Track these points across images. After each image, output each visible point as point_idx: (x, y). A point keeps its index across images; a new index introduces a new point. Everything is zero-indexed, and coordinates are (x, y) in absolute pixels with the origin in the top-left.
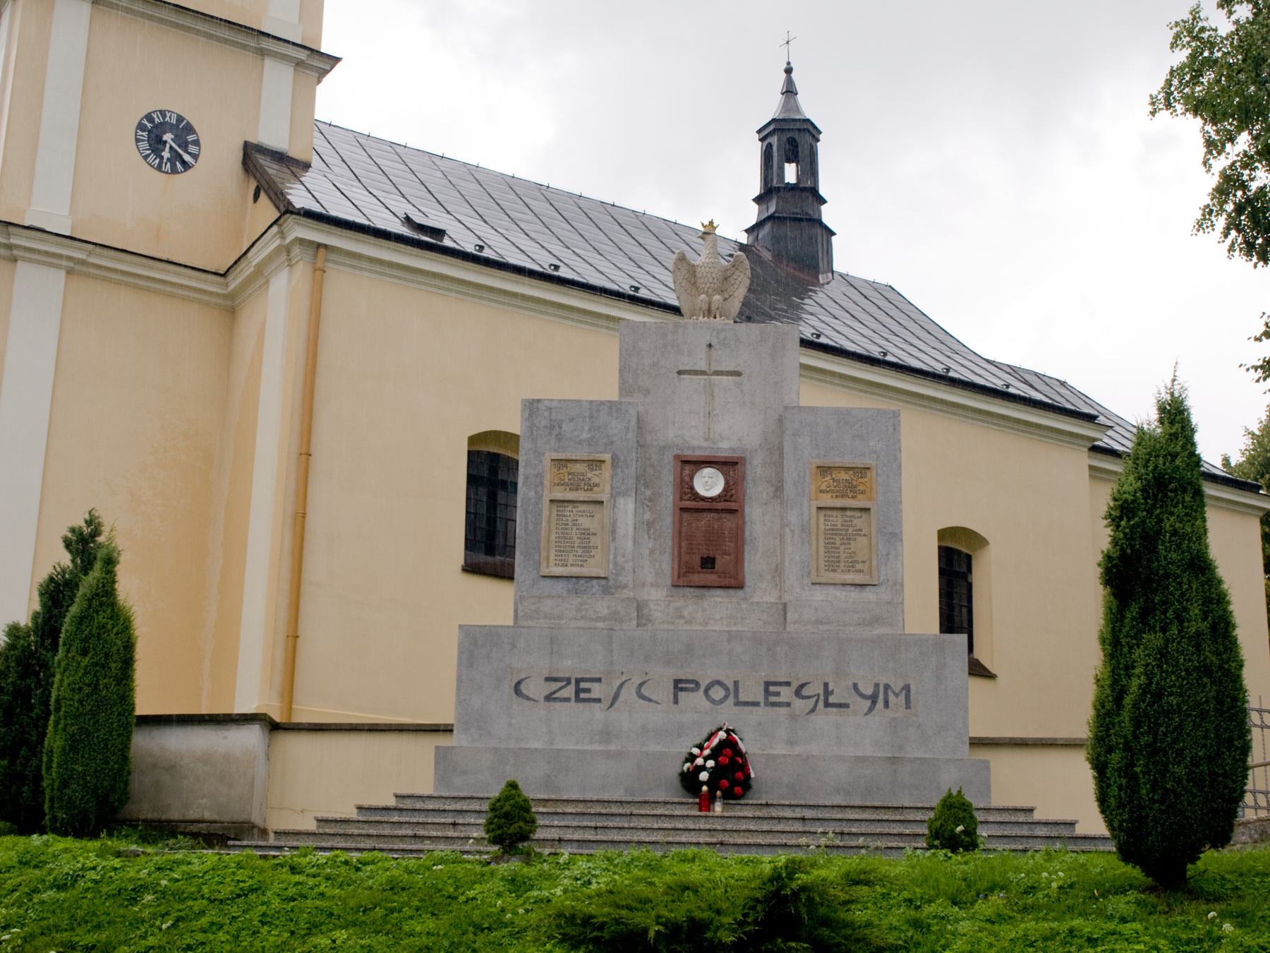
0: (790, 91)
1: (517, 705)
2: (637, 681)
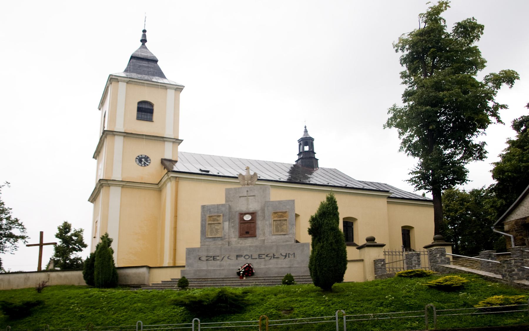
0: (306, 131)
1: (200, 262)
2: (227, 256)
